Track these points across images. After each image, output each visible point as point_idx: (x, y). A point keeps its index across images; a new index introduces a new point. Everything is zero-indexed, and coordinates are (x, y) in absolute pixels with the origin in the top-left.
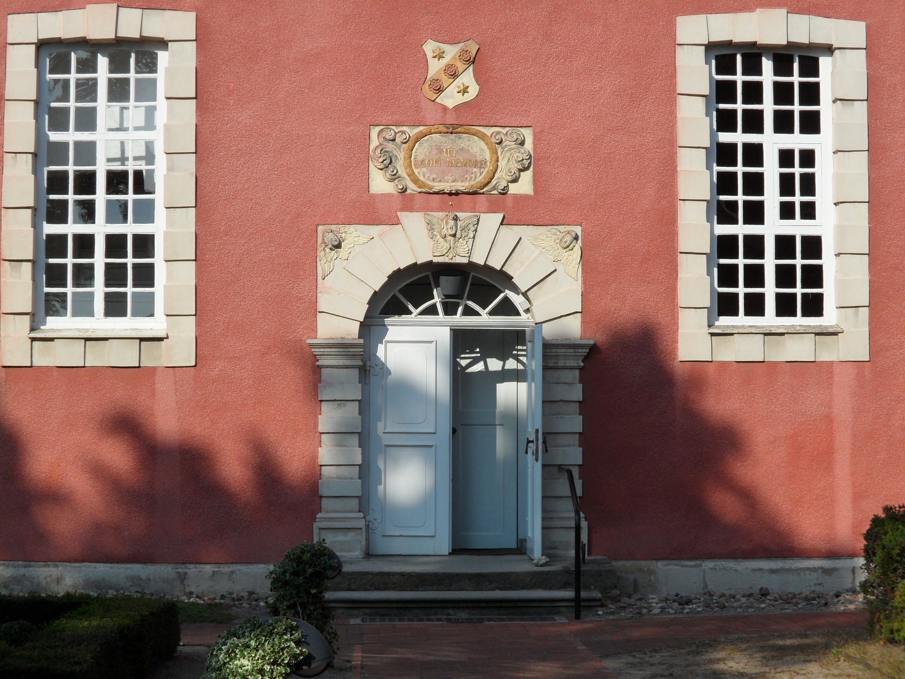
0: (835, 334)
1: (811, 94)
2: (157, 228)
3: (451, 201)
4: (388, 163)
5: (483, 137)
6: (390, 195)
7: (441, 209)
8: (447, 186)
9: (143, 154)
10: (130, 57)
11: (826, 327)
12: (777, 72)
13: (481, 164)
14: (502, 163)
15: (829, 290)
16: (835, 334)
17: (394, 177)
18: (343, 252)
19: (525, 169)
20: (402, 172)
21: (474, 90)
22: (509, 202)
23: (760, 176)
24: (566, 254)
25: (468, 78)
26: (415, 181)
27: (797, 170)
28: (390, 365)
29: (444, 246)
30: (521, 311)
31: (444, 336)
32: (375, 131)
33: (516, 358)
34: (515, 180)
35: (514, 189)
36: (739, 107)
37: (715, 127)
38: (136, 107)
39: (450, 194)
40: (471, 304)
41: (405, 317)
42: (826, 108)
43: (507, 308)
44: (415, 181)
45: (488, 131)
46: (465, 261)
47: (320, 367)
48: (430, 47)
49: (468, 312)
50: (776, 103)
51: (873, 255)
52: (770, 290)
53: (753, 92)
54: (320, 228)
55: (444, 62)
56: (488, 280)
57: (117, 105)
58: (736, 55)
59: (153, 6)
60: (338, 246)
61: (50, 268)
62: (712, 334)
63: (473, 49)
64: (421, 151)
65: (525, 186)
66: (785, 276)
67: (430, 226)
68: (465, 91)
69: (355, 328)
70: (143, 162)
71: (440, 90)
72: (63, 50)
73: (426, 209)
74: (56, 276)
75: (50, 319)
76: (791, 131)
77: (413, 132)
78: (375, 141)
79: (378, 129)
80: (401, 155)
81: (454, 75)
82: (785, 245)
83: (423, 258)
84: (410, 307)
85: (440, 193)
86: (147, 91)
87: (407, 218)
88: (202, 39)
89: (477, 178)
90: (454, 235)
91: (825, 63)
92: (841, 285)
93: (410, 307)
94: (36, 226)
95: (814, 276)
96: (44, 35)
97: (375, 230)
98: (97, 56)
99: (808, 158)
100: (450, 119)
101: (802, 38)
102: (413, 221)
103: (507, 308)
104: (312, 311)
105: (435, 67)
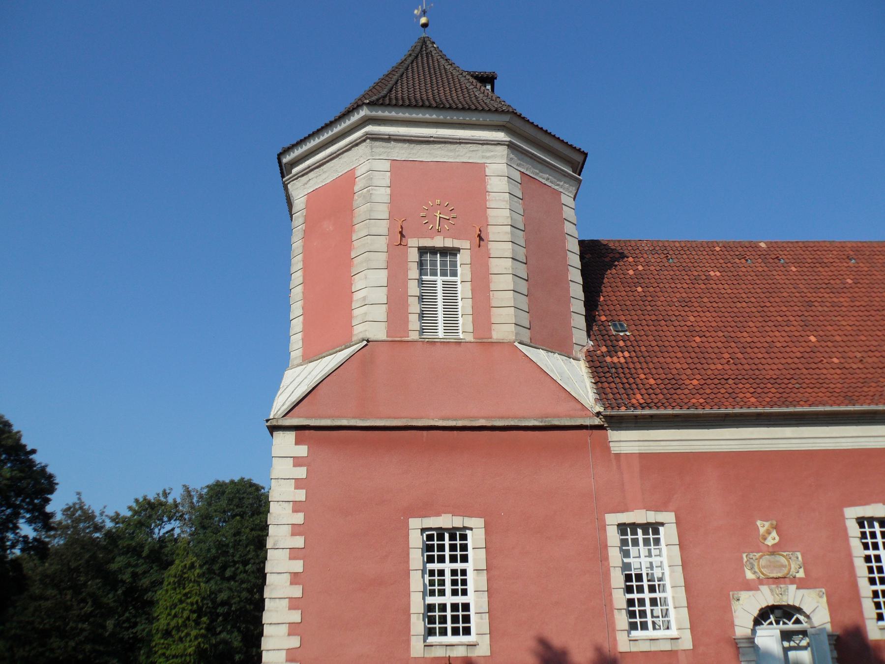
0: (475, 645)
1: (464, 548)
2: (470, 599)
3: (777, 581)
4: (752, 569)
5: (783, 556)
6: (754, 580)
7: (773, 584)
8: (774, 575)
9: (649, 566)
10: (649, 529)
11: (442, 642)
12: (643, 534)
13: (784, 566)
14: (793, 566)
15: (473, 625)
16: (475, 645)
17: (755, 573)
18: (741, 602)
19: (801, 567)
20: (757, 570)
21: (777, 539)
22: (797, 581)
23: (444, 580)
24: (820, 600)
25: (774, 534)
26: (763, 574)
27: (459, 578)
28: (760, 646)
29: (778, 598)
30: (803, 621)
31: (778, 633)
32: (744, 555)
33: (794, 641)
34: (798, 572)
35: (798, 575)
36: (436, 553)
37: (425, 560)
38: (654, 549)
39: (776, 578)
40: (785, 620)
41: (762, 626)
42: (470, 553)
43: (798, 621)
44: (763, 574)
45: (785, 554)
46: (786, 604)
47: (739, 648)
48: (759, 523)
49: (784, 623)
50: (450, 551)
51: (689, 607)
52: (449, 625)
53: (441, 548)
54: (731, 593)
55: (765, 528)
56: (788, 610)
57: (647, 548)
58: (627, 528)
59: (658, 510)
60: (738, 600)
61: (429, 617)
62: (630, 640)
63: (775, 523)
64: (763, 562)
65: (801, 574)
66: (455, 619)
67: (771, 590)
68: (774, 539)
69: (749, 631)
70: (649, 569)
71: (765, 539)
72: (624, 527)
73: (768, 584)
74: (431, 620)
75: (429, 638)
76: (457, 562)
77: (758, 555)
78: (745, 559)
79: (746, 554)
80: (756, 564)
81: (769, 533)
82: (455, 607)
83: (770, 604)
84: (763, 622)
85: (773, 578)
86: (657, 542)
87: (761, 587)
88: (678, 523)
89: (785, 571)
90: (781, 594)
91: (661, 529)
92: (477, 625)
93: (763, 622)
94: (424, 599)
95: (467, 619)
96: (424, 527)
97: (751, 593)
98: (637, 530)
99: (464, 573)
100: (771, 550)
101: (652, 521)
102: (765, 589)
103: (798, 621)
104: (732, 625)
105: (762, 530)
